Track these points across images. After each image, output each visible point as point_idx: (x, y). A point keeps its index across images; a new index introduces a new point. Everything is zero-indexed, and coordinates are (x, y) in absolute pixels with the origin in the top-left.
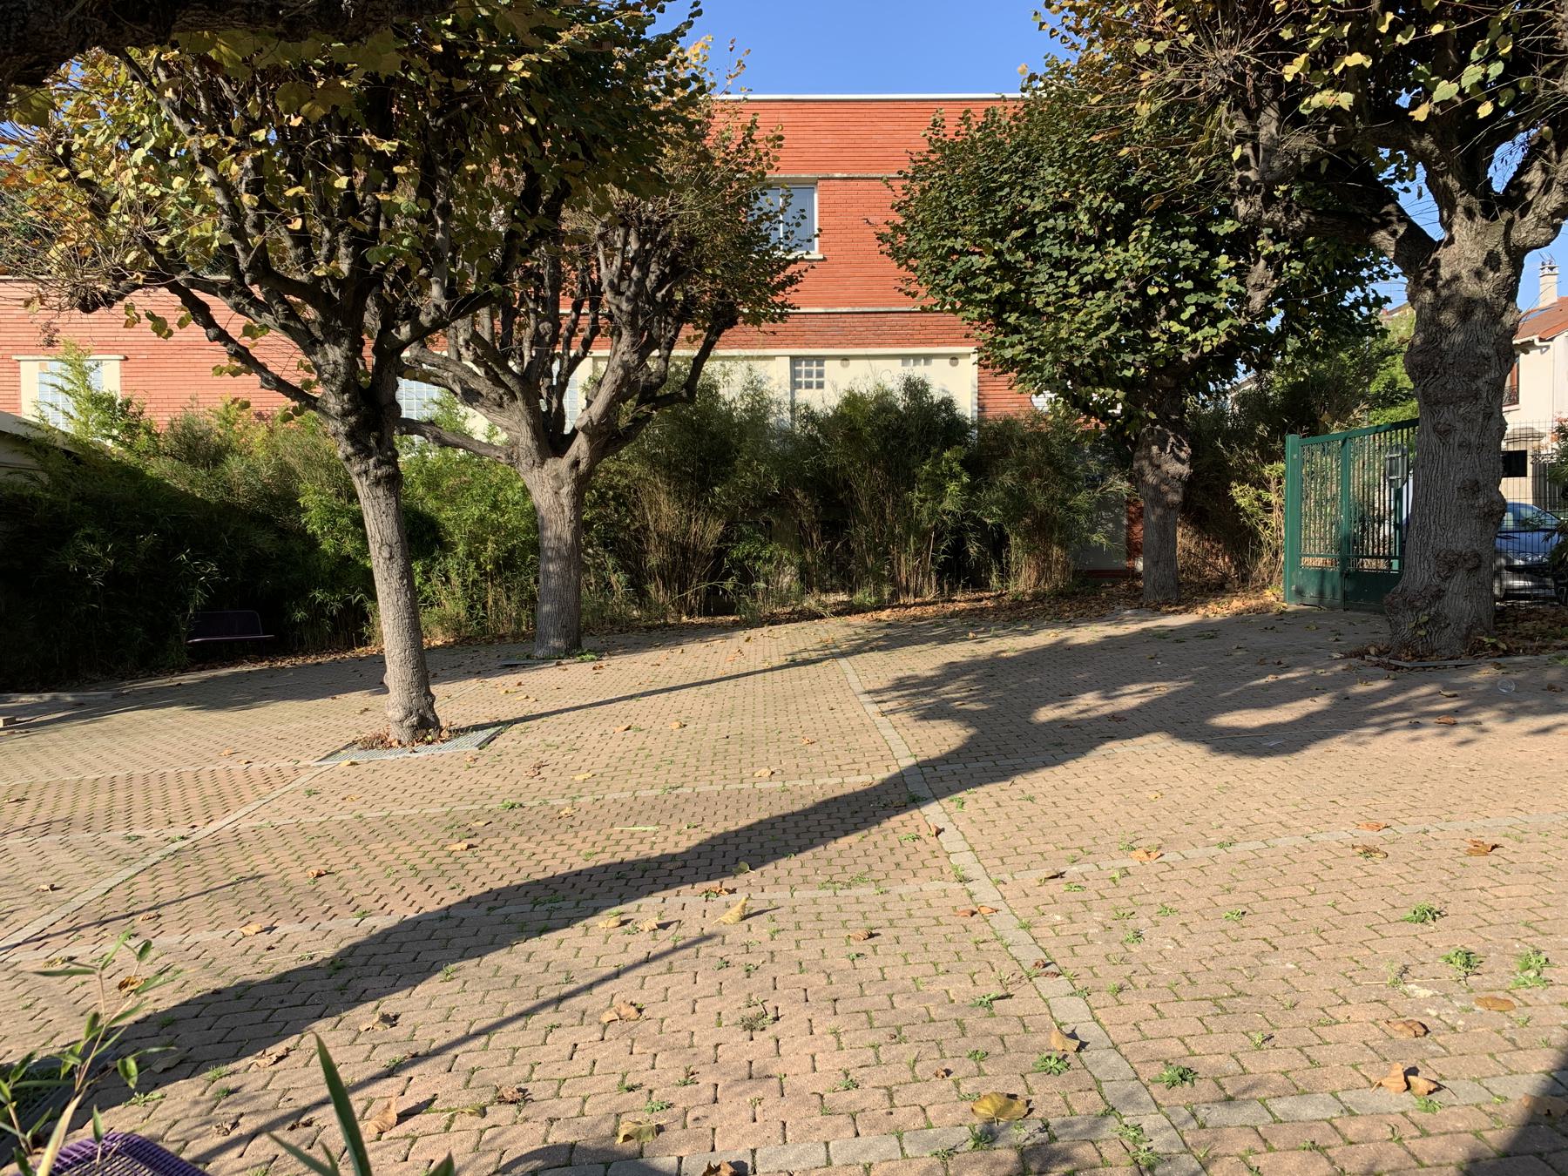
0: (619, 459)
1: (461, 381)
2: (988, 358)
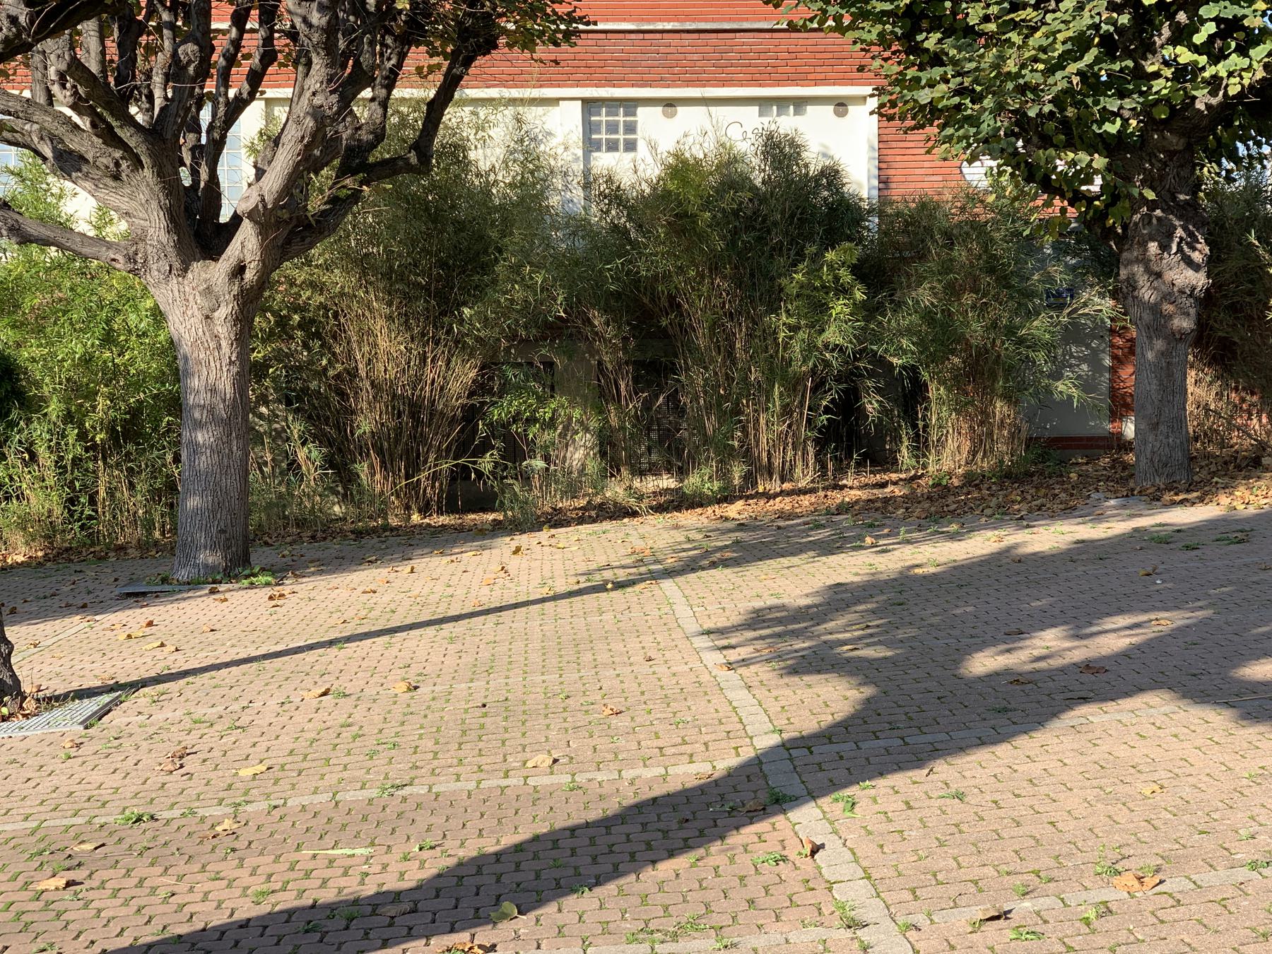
0: (308, 263)
1: (53, 138)
2: (893, 104)
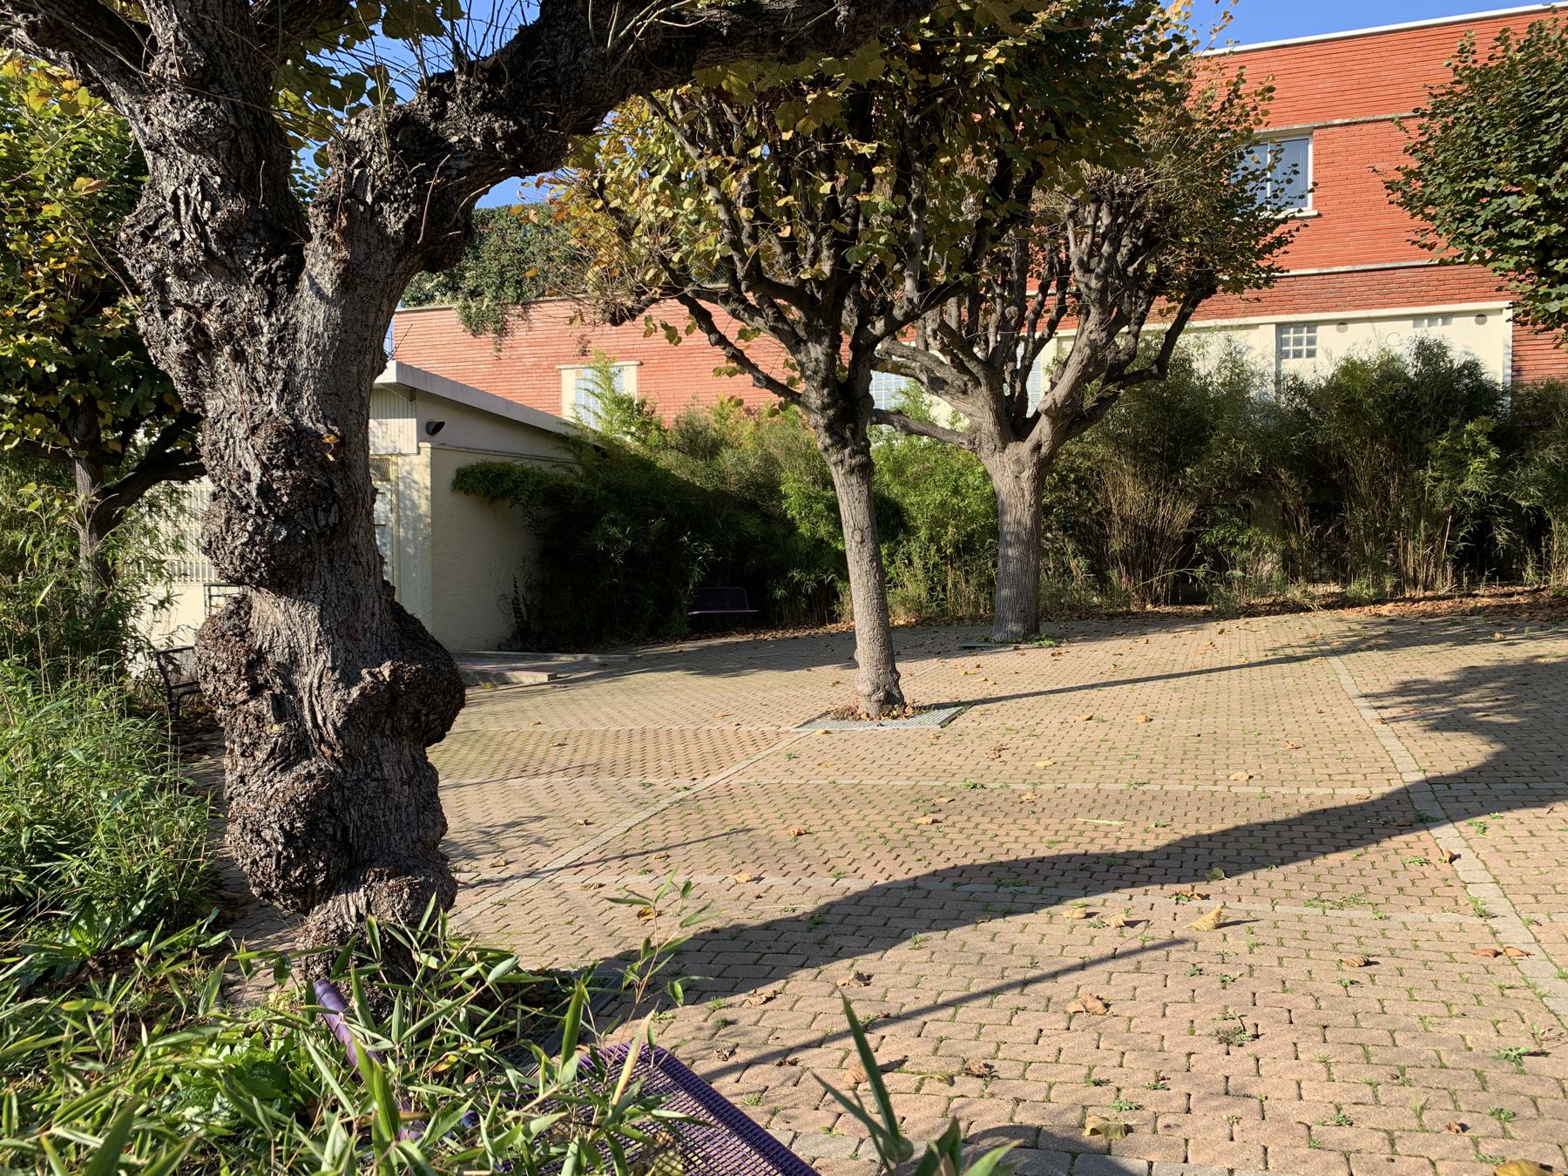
0: (1081, 440)
1: (928, 371)
2: (1527, 313)
